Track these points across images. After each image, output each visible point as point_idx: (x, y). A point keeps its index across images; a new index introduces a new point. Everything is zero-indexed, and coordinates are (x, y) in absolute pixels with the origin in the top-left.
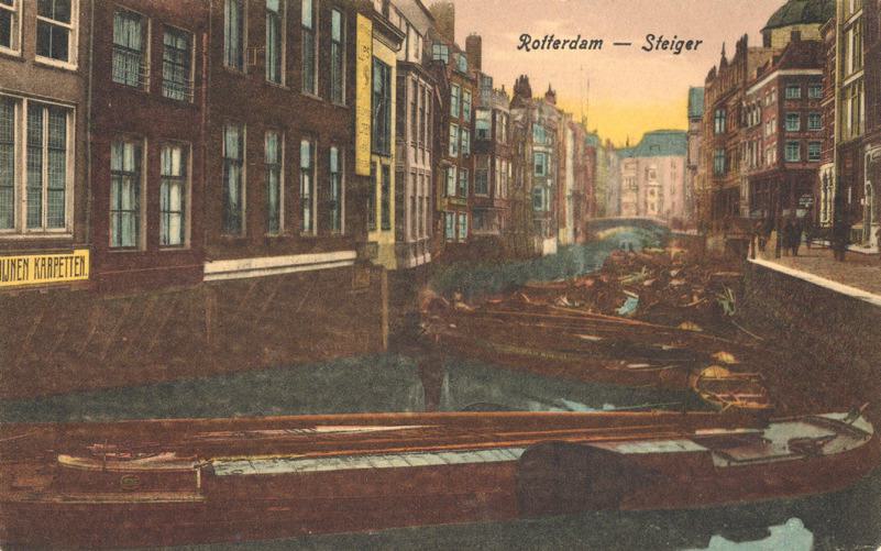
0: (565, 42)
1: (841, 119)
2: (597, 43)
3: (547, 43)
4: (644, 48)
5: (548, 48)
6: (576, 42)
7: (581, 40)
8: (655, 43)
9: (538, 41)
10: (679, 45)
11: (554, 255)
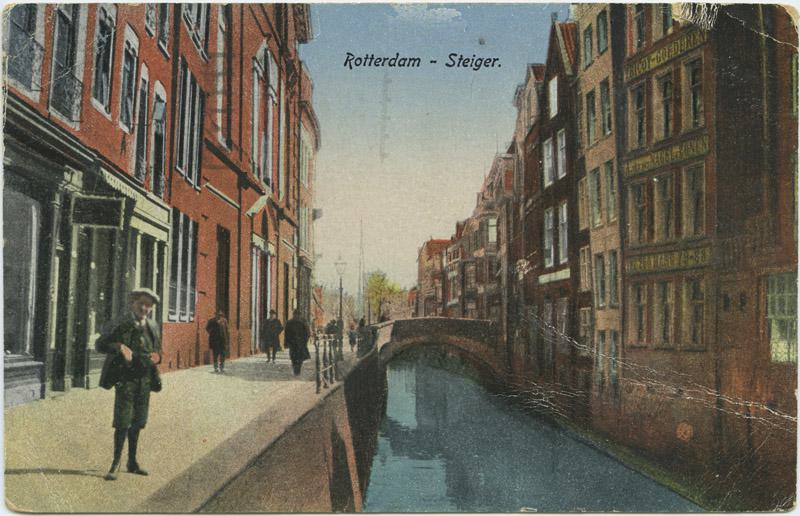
0: (385, 59)
1: (61, 128)
2: (416, 61)
3: (368, 60)
4: (447, 65)
5: (370, 65)
6: (396, 59)
7: (400, 58)
8: (456, 59)
9: (360, 59)
10: (479, 62)
11: (769, 358)
